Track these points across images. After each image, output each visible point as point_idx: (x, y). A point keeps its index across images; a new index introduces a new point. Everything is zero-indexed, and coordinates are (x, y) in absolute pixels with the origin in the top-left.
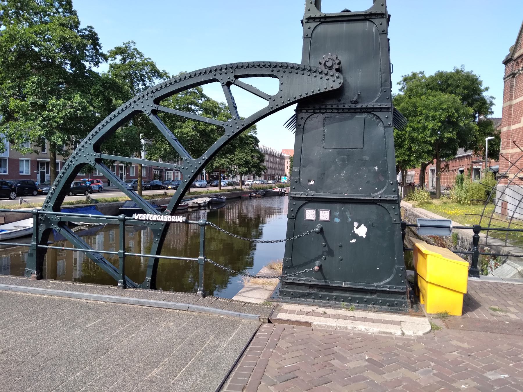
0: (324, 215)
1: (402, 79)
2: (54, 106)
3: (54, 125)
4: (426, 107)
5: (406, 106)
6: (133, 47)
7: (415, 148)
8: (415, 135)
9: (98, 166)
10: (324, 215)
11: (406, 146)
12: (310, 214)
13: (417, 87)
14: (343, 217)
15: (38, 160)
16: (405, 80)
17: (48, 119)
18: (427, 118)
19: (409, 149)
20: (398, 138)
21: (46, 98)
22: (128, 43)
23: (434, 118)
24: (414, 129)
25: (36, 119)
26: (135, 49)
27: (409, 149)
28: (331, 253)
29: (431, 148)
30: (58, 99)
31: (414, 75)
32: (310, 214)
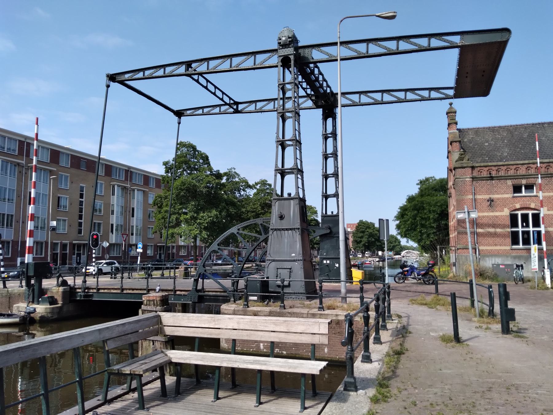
0: (328, 262)
1: (419, 182)
2: (203, 217)
3: (203, 227)
4: (429, 204)
5: (416, 203)
6: (234, 171)
7: (424, 230)
8: (423, 222)
9: (219, 251)
10: (328, 262)
11: (418, 230)
12: (325, 262)
13: (426, 189)
14: (333, 263)
15: (74, 242)
16: (421, 182)
17: (200, 224)
18: (430, 211)
19: (420, 232)
20: (412, 225)
21: (198, 213)
22: (231, 169)
23: (434, 211)
24: (422, 218)
25: (194, 224)
26: (235, 172)
27: (420, 232)
28: (330, 271)
29: (435, 231)
30: (204, 212)
31: (427, 179)
32: (325, 262)
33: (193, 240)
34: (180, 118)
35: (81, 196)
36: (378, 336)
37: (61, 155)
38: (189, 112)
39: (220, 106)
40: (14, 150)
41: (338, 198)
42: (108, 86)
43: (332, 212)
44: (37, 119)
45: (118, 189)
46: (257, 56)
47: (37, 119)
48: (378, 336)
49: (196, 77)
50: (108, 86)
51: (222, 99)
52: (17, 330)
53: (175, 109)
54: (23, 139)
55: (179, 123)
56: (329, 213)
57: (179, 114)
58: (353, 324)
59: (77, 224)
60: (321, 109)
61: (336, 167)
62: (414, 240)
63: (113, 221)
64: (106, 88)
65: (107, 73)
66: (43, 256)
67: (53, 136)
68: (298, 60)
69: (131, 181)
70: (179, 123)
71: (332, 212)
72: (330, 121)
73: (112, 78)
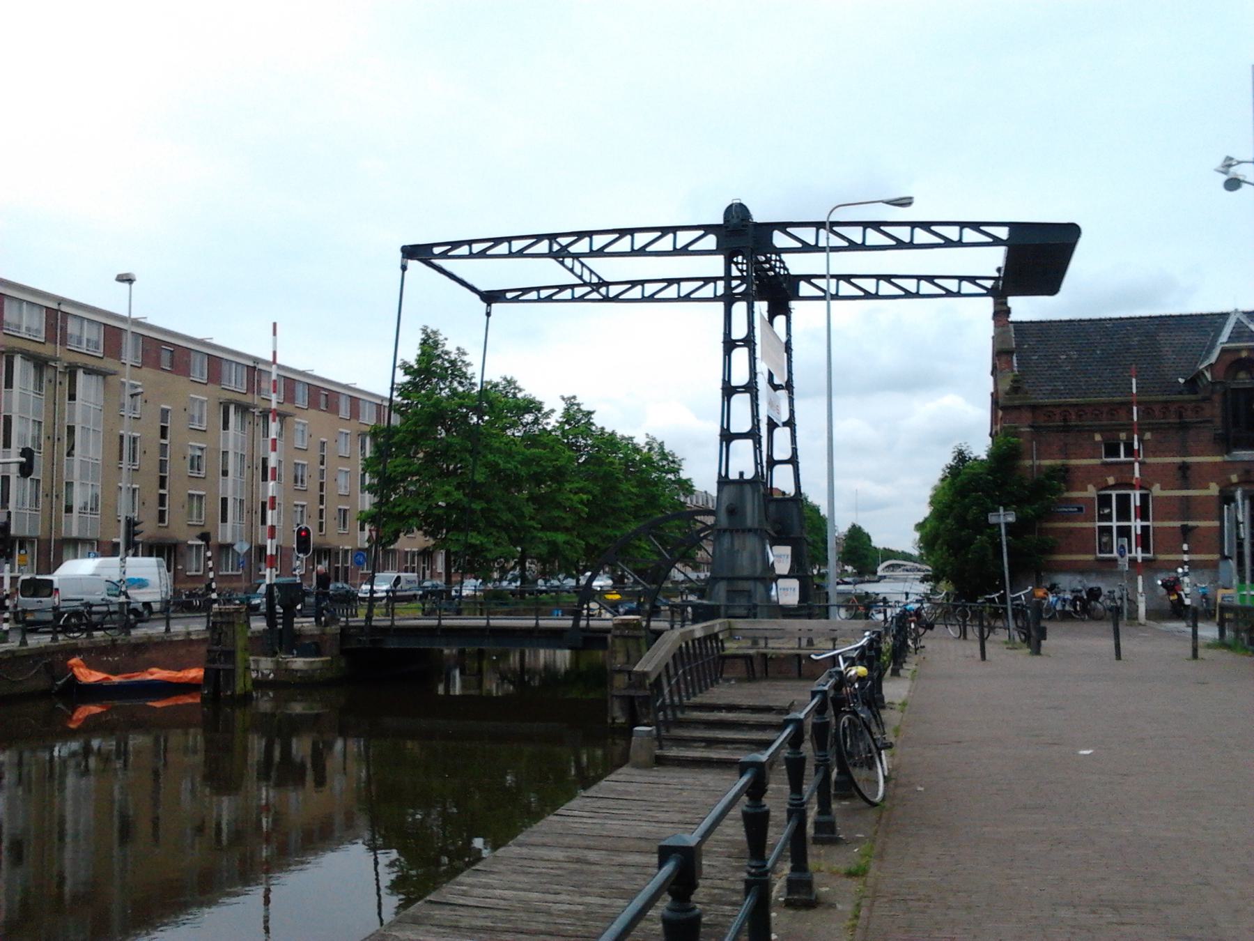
33: (137, 539)
34: (489, 305)
35: (164, 432)
36: (826, 818)
37: (225, 367)
38: (509, 295)
39: (572, 287)
40: (38, 331)
41: (770, 456)
42: (404, 268)
43: (741, 474)
44: (275, 325)
45: (24, 372)
46: (679, 233)
47: (275, 325)
48: (826, 818)
49: (568, 261)
50: (404, 268)
51: (580, 277)
52: (1138, 504)
53: (483, 287)
54: (55, 306)
55: (488, 314)
56: (734, 475)
57: (491, 297)
58: (694, 886)
59: (156, 500)
60: (721, 222)
61: (792, 412)
62: (98, 670)
63: (225, 490)
64: (400, 271)
65: (859, 523)
66: (201, 573)
67: (299, 356)
68: (741, 235)
69: (259, 393)
70: (488, 314)
71: (741, 474)
72: (780, 320)
73: (411, 252)
